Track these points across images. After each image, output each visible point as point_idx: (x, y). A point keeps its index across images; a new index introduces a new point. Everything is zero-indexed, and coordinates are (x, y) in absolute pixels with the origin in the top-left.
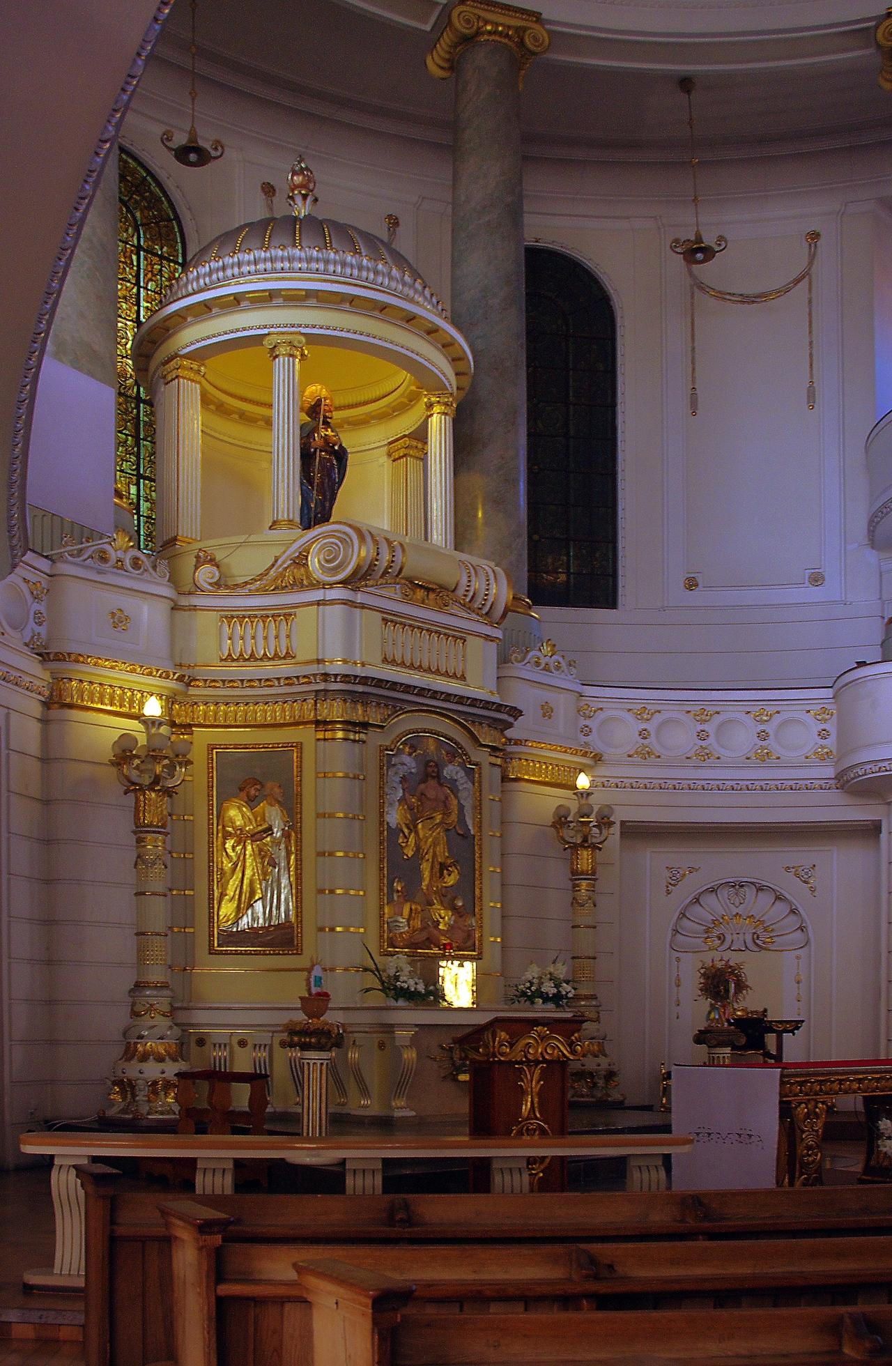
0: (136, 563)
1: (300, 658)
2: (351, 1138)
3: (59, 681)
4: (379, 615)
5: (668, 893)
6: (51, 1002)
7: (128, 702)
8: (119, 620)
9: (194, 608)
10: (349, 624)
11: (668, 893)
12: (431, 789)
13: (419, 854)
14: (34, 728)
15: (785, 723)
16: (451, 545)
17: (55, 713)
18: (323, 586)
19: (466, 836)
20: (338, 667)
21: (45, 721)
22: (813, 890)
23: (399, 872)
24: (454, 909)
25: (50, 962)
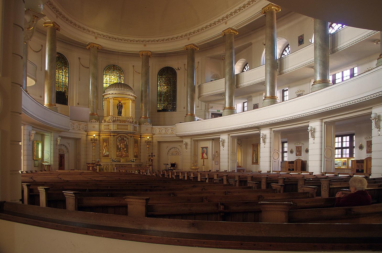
0: (95, 121)
1: (117, 125)
2: (48, 101)
3: (87, 133)
4: (117, 125)
5: (67, 143)
6: (87, 148)
7: (94, 135)
8: (94, 127)
9: (102, 125)
10: (113, 126)
11: (67, 143)
12: (122, 141)
13: (121, 147)
14: (85, 138)
15: (162, 130)
16: (58, 167)
17: (87, 136)
18: (111, 122)
19: (127, 145)
20: (112, 130)
21: (86, 137)
22: (181, 148)
23: (118, 149)
24: (125, 152)
25: (86, 144)
